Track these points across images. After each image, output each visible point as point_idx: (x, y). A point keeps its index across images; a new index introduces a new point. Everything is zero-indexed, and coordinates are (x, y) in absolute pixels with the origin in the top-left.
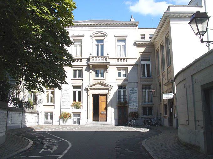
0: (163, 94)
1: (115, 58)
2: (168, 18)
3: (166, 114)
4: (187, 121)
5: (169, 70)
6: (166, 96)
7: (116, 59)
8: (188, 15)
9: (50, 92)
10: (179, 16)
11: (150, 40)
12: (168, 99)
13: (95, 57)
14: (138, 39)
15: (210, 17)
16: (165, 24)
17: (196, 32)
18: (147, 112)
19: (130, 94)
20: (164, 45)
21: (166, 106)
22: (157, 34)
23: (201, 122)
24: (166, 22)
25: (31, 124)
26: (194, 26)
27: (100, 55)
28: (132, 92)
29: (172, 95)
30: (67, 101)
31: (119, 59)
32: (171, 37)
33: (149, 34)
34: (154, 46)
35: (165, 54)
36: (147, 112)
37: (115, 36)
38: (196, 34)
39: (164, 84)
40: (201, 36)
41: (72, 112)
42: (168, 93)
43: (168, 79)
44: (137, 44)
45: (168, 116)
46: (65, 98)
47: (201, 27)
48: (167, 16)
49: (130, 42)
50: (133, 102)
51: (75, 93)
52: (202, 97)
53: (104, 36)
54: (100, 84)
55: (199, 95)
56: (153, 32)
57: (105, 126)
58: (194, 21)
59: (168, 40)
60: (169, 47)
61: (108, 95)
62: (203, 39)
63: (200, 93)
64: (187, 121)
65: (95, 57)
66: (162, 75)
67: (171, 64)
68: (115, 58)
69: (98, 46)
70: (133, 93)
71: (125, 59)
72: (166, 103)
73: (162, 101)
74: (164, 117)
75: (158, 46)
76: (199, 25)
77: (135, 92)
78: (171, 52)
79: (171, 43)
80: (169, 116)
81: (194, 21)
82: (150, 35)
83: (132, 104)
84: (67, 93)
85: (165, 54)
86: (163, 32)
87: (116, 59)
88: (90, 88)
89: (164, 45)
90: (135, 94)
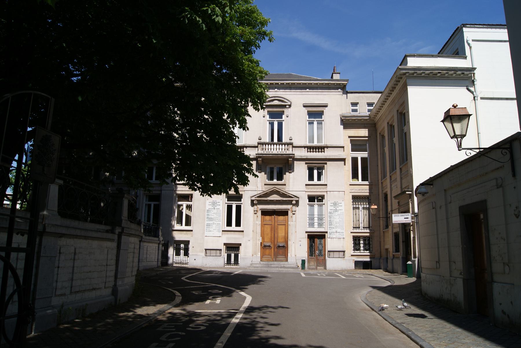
0: (393, 215)
1: (305, 147)
2: (403, 78)
3: (397, 250)
4: (437, 262)
5: (404, 169)
6: (398, 218)
7: (306, 149)
8: (439, 73)
9: (184, 207)
10: (423, 75)
11: (368, 114)
12: (402, 224)
13: (268, 144)
14: (347, 110)
15: (471, 115)
16: (398, 88)
17: (452, 135)
18: (362, 245)
19: (330, 213)
20: (395, 124)
21: (396, 235)
22: (382, 103)
23: (459, 265)
24: (400, 85)
25: (293, 249)
26: (449, 125)
27: (276, 140)
28: (334, 209)
29: (409, 215)
30: (215, 222)
31: (310, 148)
32: (408, 112)
33: (364, 104)
34: (375, 124)
35: (396, 140)
36: (362, 245)
37: (304, 106)
38: (452, 138)
39: (393, 196)
40: (459, 139)
41: (225, 244)
42: (402, 213)
43: (401, 187)
44: (347, 123)
45: (400, 254)
46: (212, 217)
47: (458, 127)
48: (401, 75)
49: (332, 118)
50: (336, 227)
51: (230, 208)
52: (461, 224)
53: (284, 106)
54: (277, 193)
55: (456, 222)
56: (375, 98)
57: (284, 270)
58: (449, 118)
59: (403, 117)
60: (405, 128)
61: (291, 214)
62: (461, 144)
63: (458, 218)
64: (437, 262)
65: (268, 144)
66: (391, 179)
67: (407, 160)
68: (305, 147)
69: (272, 124)
70: (336, 210)
71: (321, 149)
72: (396, 230)
73: (390, 227)
74: (393, 255)
75: (383, 127)
76: (455, 125)
77: (340, 208)
78: (407, 139)
79: (409, 122)
80: (403, 254)
81: (449, 118)
82: (370, 104)
83: (334, 230)
84: (216, 208)
85: (396, 140)
86: (393, 101)
87: (306, 149)
88: (257, 200)
89: (395, 124)
90: (339, 213)
